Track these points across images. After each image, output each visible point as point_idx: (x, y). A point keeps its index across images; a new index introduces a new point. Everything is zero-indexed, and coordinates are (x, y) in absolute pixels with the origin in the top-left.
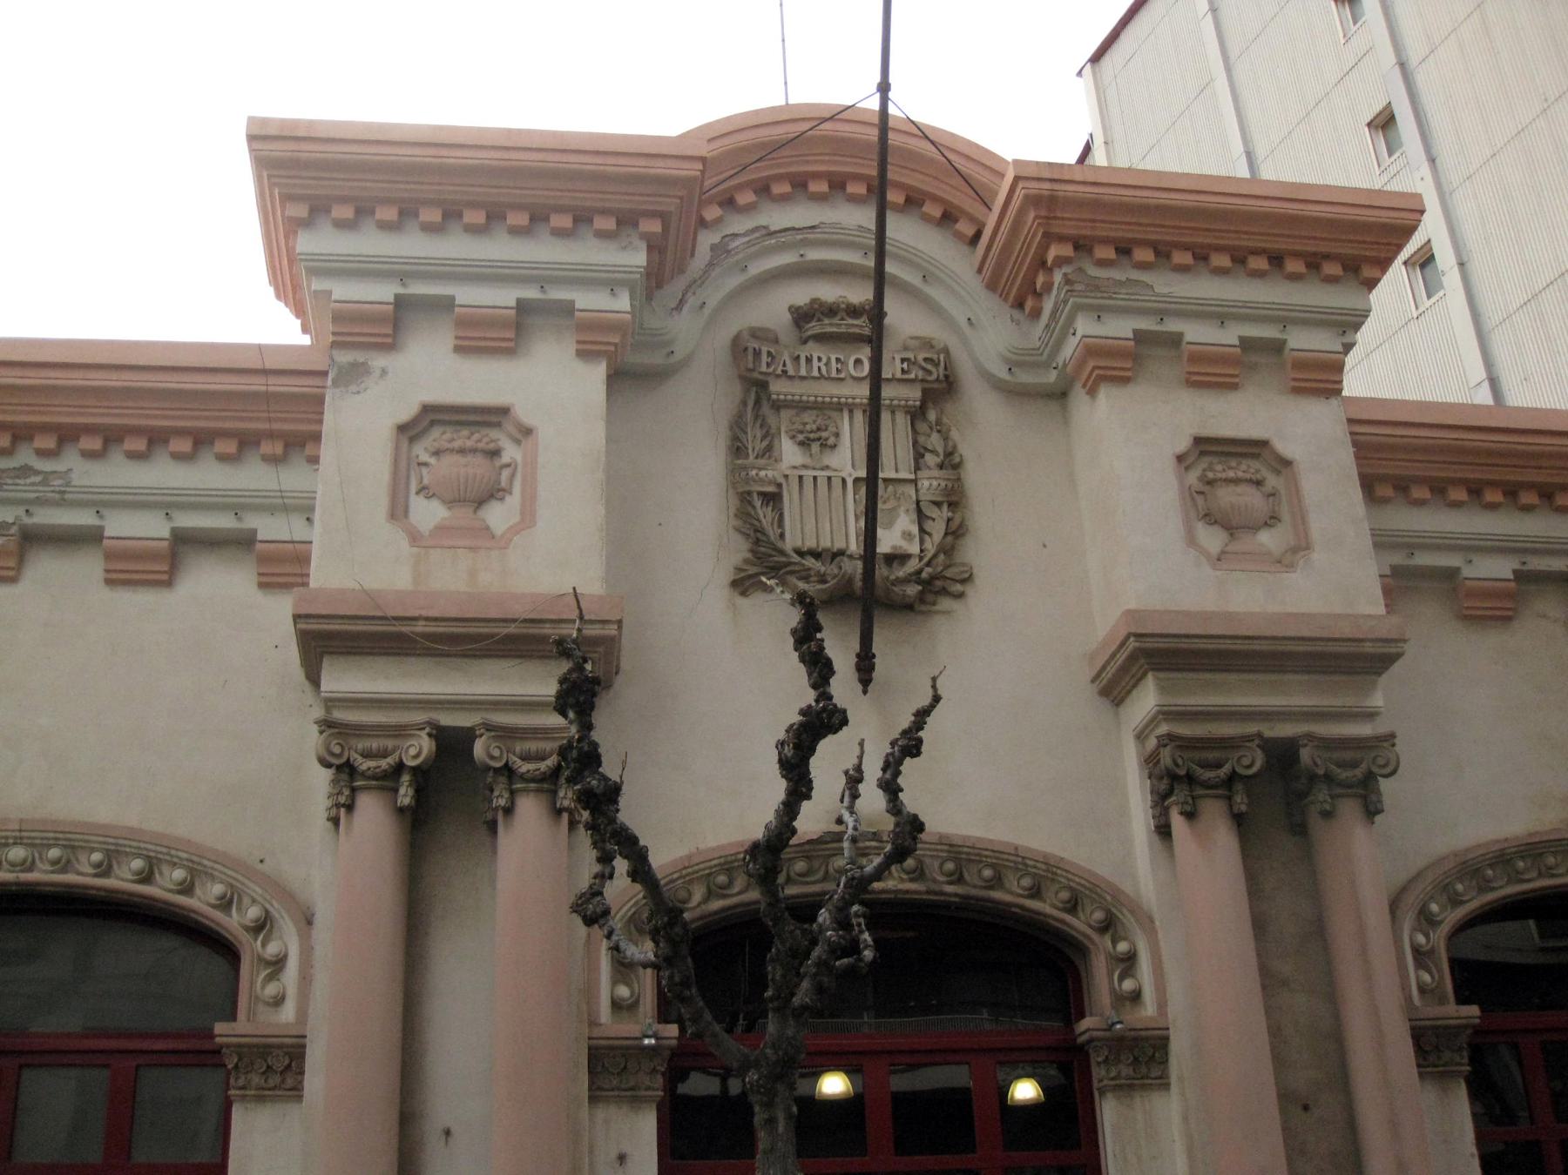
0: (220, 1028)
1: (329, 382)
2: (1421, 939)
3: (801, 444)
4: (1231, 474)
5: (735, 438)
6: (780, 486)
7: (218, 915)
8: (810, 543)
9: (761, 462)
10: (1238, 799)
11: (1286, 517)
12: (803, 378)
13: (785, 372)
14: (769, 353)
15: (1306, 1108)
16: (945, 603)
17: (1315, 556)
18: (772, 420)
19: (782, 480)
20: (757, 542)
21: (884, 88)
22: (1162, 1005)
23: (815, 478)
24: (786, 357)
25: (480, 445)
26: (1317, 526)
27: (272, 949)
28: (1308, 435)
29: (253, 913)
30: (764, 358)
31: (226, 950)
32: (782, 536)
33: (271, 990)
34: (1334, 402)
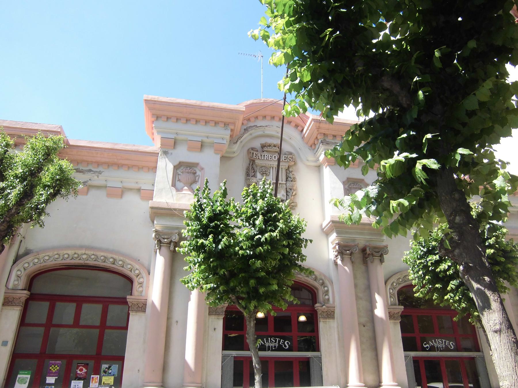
0: (128, 297)
5: (247, 172)
15: (364, 326)
18: (255, 168)
22: (334, 302)
24: (259, 155)
27: (141, 280)
29: (137, 272)
30: (254, 155)
33: (141, 289)
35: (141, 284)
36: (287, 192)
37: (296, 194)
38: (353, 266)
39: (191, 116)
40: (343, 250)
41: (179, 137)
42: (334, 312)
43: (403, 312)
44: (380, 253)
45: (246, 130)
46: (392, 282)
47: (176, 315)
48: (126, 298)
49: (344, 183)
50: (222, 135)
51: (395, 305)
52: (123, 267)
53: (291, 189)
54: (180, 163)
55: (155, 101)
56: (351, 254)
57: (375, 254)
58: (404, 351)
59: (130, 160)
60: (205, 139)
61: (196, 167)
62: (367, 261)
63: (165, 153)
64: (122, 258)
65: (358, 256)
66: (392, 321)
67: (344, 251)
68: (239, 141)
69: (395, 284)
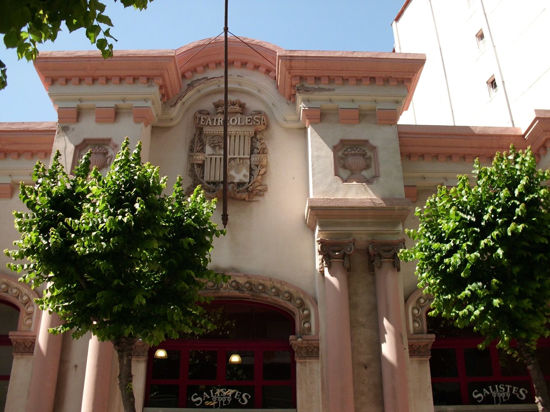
0: (11, 333)
1: (56, 133)
2: (416, 311)
3: (213, 147)
4: (353, 152)
5: (191, 146)
6: (204, 161)
7: (276, 298)
8: (212, 179)
9: (198, 153)
10: (346, 262)
11: (373, 165)
12: (215, 126)
13: (208, 124)
14: (204, 118)
15: (366, 368)
16: (257, 198)
17: (380, 179)
18: (204, 140)
19: (205, 159)
20: (195, 180)
21: (226, 29)
22: (317, 331)
23: (211, 158)
24: (209, 119)
25: (102, 151)
26: (382, 169)
27: (30, 309)
28: (381, 138)
29: (25, 298)
30: (202, 120)
31: (17, 309)
32: (203, 178)
33: (28, 322)
34: (394, 126)
35: (30, 314)
36: (251, 170)
37: (265, 173)
38: (349, 278)
39: (98, 73)
40: (328, 251)
41: (85, 104)
42: (318, 348)
43: (434, 344)
44: (392, 253)
45: (191, 86)
46: (418, 296)
47: (74, 359)
48: (8, 336)
49: (335, 149)
50: (147, 96)
51: (422, 333)
52: (7, 292)
53: (257, 166)
54: (85, 140)
55: (47, 58)
56: (344, 256)
57: (384, 254)
58: (435, 404)
59: (18, 143)
60: (120, 104)
61: (108, 145)
62: (373, 266)
63: (65, 129)
64: (5, 280)
65: (360, 261)
66: (415, 359)
67: (331, 253)
68: (180, 103)
69: (422, 301)
